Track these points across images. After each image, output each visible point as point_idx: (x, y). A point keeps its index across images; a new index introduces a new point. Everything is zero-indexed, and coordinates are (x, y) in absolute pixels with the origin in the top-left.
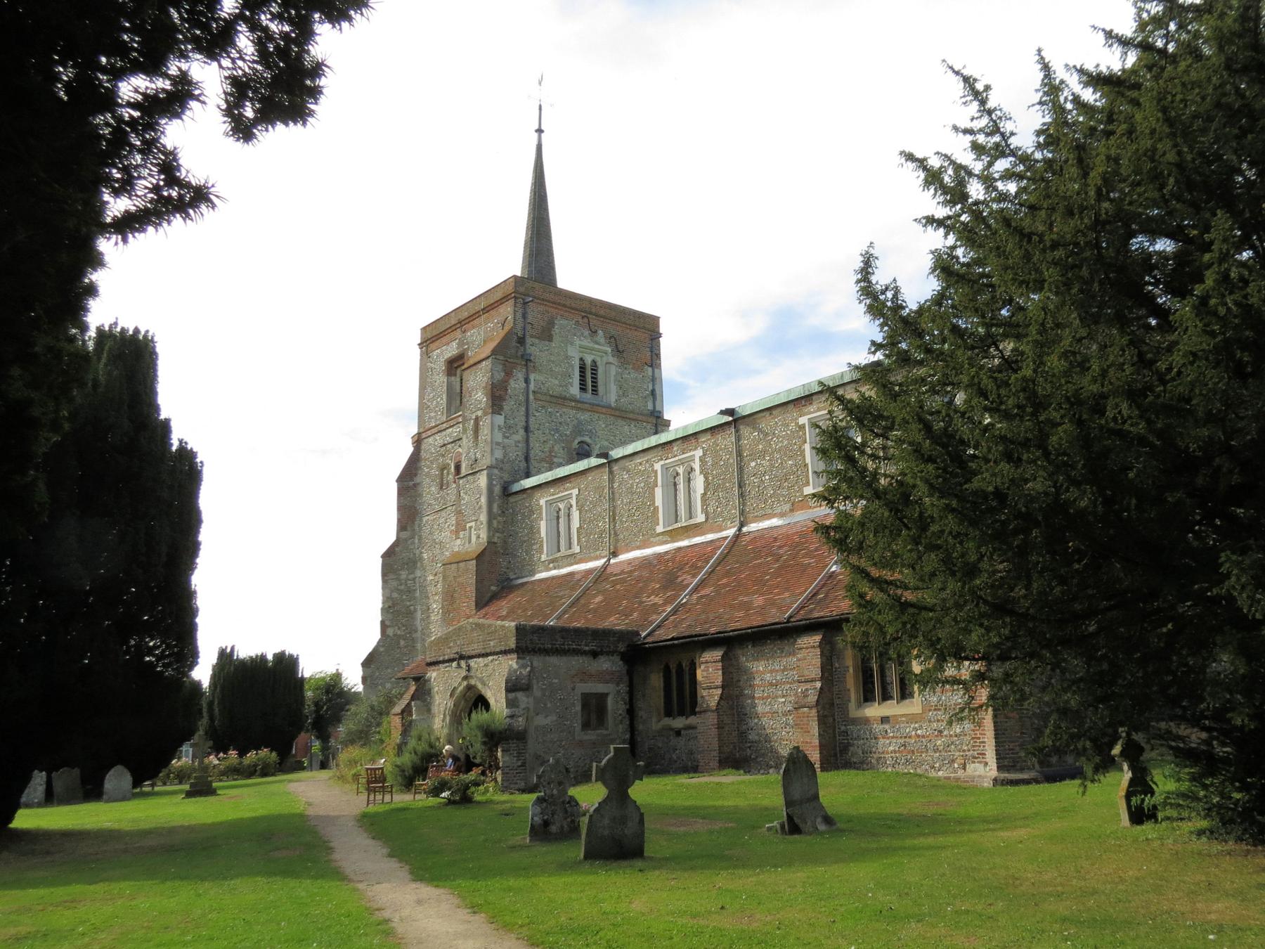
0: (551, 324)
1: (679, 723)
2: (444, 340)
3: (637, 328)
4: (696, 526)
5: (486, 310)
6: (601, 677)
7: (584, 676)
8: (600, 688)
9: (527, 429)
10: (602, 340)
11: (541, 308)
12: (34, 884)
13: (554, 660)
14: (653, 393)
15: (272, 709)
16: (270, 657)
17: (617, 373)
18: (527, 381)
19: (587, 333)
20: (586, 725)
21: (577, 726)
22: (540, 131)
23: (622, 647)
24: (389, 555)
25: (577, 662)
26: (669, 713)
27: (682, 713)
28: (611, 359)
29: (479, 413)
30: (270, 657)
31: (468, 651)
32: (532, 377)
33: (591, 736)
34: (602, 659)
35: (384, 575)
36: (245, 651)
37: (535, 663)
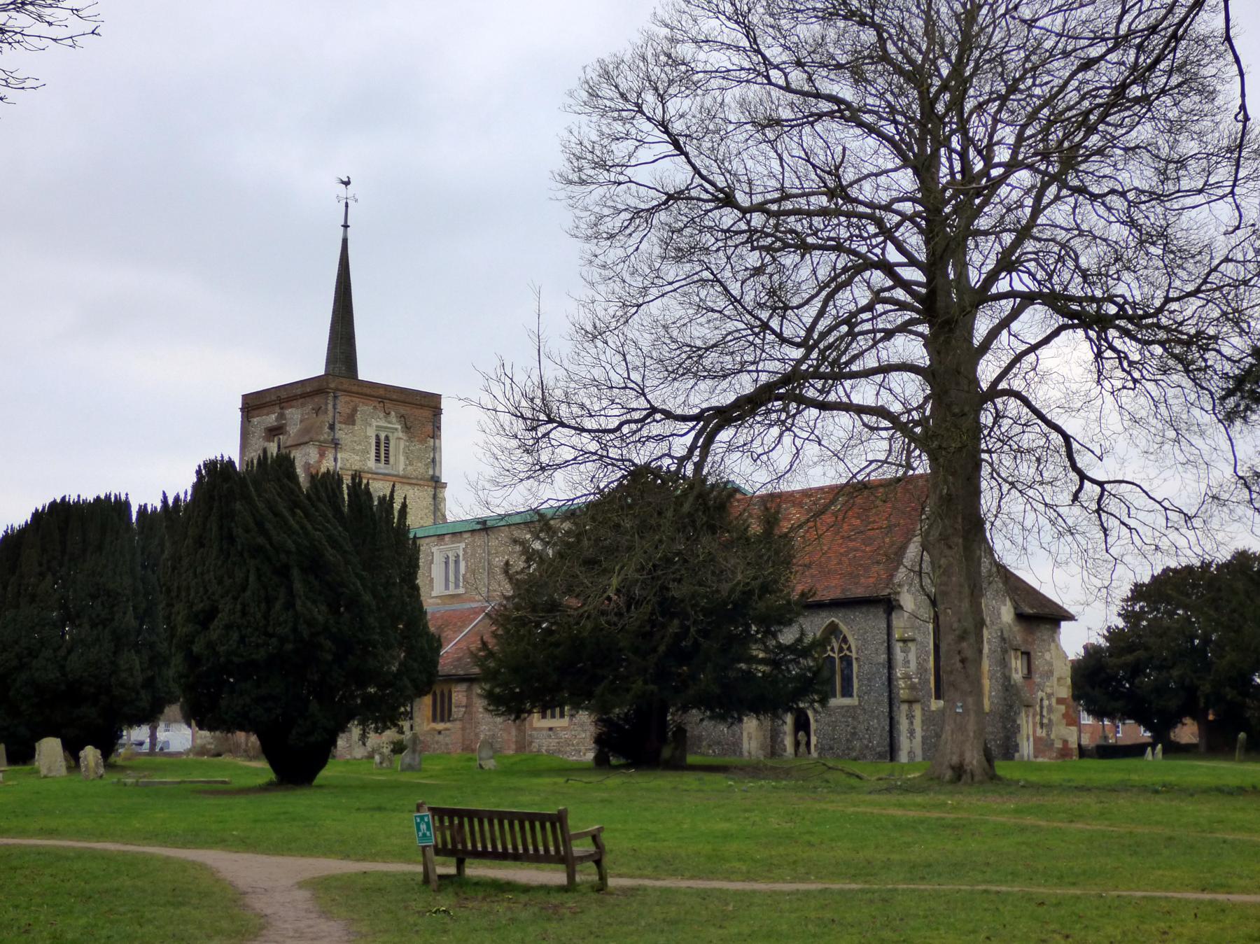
0: (355, 410)
1: (440, 726)
2: (265, 411)
3: (422, 406)
4: (459, 595)
5: (304, 396)
10: (394, 420)
11: (348, 399)
12: (506, 867)
14: (434, 461)
16: (1121, 623)
17: (406, 446)
18: (335, 460)
19: (382, 415)
26: (434, 720)
27: (442, 720)
28: (401, 435)
30: (1121, 623)
32: (339, 456)
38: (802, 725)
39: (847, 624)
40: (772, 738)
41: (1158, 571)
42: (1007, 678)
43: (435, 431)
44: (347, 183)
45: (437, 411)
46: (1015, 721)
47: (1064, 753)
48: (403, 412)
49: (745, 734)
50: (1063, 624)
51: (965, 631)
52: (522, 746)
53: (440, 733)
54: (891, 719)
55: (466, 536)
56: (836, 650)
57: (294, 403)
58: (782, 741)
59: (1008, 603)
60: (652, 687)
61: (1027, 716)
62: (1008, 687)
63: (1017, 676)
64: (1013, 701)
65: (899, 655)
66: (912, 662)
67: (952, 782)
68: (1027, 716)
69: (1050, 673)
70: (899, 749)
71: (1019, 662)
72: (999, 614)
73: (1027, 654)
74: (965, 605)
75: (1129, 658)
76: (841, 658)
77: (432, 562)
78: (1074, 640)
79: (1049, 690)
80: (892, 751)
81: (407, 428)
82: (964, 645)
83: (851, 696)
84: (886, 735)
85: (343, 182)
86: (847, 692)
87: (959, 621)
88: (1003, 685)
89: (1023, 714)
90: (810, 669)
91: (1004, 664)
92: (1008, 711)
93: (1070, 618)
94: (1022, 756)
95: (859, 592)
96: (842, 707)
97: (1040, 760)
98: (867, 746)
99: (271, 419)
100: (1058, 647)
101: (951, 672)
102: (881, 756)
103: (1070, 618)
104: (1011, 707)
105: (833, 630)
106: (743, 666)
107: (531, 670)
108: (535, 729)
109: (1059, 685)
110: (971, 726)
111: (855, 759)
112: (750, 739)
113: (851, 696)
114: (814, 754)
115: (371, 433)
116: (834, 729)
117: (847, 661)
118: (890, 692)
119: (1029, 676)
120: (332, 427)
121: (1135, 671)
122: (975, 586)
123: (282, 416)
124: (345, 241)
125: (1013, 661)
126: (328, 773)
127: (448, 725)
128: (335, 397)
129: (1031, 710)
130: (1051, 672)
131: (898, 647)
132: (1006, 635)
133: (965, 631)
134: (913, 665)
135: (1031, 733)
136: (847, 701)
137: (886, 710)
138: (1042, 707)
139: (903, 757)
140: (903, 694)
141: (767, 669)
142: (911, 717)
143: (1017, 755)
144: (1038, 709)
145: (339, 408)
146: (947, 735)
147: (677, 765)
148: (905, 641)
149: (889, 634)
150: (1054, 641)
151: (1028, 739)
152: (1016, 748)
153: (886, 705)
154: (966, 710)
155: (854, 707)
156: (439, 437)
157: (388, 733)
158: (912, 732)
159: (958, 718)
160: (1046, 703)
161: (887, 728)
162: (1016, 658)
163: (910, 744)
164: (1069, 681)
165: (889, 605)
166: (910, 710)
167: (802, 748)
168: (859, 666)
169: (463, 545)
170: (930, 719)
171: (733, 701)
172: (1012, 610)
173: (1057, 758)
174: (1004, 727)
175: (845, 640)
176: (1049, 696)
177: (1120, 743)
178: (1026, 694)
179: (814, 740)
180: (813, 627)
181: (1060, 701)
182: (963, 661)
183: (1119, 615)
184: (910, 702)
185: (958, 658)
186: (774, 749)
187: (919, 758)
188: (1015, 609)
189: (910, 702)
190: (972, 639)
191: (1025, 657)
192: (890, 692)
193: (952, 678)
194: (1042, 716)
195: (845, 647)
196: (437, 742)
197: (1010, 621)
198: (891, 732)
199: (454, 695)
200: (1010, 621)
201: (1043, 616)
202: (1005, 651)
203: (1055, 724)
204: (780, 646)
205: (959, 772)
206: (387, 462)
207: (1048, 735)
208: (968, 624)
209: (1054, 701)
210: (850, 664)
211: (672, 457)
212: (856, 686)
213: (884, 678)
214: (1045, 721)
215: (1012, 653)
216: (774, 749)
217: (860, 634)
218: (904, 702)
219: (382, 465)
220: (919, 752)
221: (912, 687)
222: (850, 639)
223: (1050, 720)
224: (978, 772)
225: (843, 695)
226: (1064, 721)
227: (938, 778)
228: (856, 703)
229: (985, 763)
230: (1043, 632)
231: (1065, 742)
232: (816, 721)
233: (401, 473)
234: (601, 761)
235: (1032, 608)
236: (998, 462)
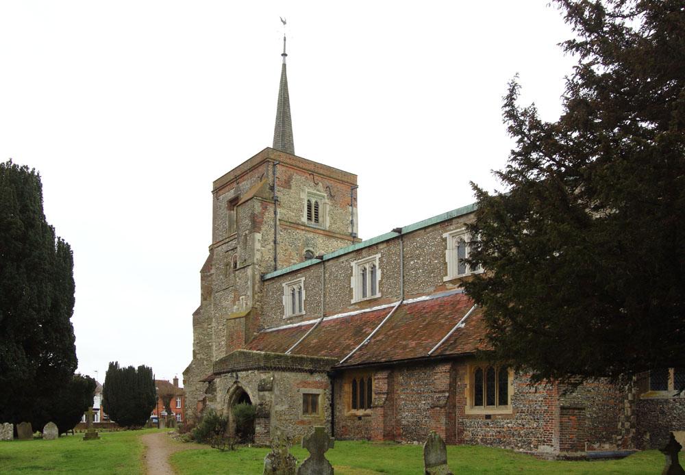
1: (360, 412)
2: (227, 189)
6: (316, 385)
7: (305, 384)
10: (322, 189)
13: (287, 374)
14: (352, 222)
15: (133, 394)
16: (136, 368)
19: (312, 184)
21: (300, 412)
22: (284, 55)
23: (328, 369)
24: (196, 314)
25: (300, 376)
26: (355, 407)
27: (362, 407)
28: (327, 201)
29: (247, 232)
30: (136, 368)
31: (237, 367)
32: (278, 210)
33: (307, 418)
35: (194, 326)
36: (123, 364)
37: (276, 376)
43: (353, 201)
45: (354, 187)
48: (328, 184)
53: (360, 418)
55: (381, 247)
57: (246, 177)
77: (351, 275)
81: (331, 196)
99: (230, 194)
108: (468, 417)
115: (304, 196)
120: (272, 188)
123: (237, 189)
124: (284, 66)
127: (368, 411)
128: (274, 165)
145: (278, 175)
147: (269, 413)
156: (356, 206)
157: (212, 407)
169: (379, 255)
199: (374, 383)
206: (317, 220)
219: (313, 222)
233: (327, 229)
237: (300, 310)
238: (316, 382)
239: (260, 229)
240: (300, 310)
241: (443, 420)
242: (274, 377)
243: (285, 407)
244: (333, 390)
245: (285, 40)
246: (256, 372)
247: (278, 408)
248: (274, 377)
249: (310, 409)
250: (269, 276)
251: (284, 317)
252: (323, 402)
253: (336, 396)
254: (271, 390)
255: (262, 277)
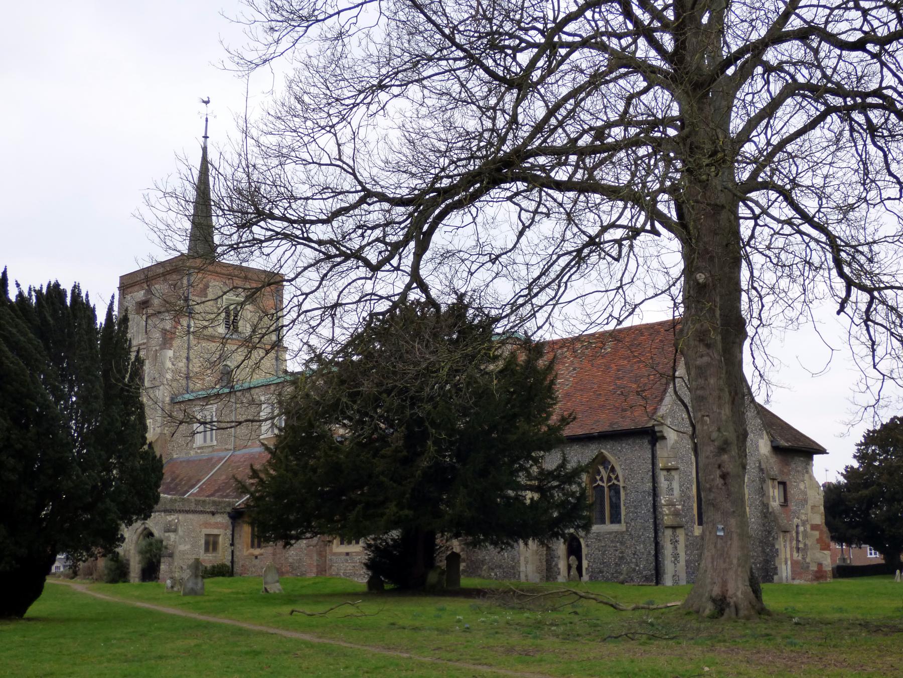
6: (216, 526)
7: (206, 525)
8: (215, 532)
9: (188, 359)
13: (190, 516)
16: (856, 465)
20: (207, 550)
21: (202, 551)
22: (206, 137)
23: (229, 509)
25: (202, 518)
26: (252, 546)
29: (158, 348)
30: (856, 465)
34: (217, 516)
37: (180, 518)
38: (574, 549)
39: (614, 455)
40: (547, 561)
41: (886, 420)
42: (766, 506)
44: (207, 102)
46: (773, 546)
47: (819, 575)
49: (522, 558)
50: (816, 457)
51: (726, 442)
52: (322, 570)
53: (256, 557)
54: (657, 544)
56: (605, 479)
58: (557, 565)
59: (765, 436)
60: (406, 512)
61: (785, 541)
62: (766, 513)
63: (775, 504)
64: (772, 527)
65: (663, 483)
66: (676, 490)
67: (712, 617)
68: (785, 541)
69: (805, 501)
70: (664, 573)
71: (776, 491)
72: (757, 447)
73: (783, 484)
74: (726, 411)
75: (865, 492)
76: (609, 487)
78: (829, 470)
79: (803, 517)
80: (657, 576)
82: (725, 457)
83: (619, 522)
84: (652, 558)
85: (204, 102)
86: (615, 518)
87: (719, 430)
88: (762, 512)
89: (781, 539)
90: (573, 494)
91: (762, 492)
92: (767, 537)
93: (822, 451)
94: (781, 578)
95: (626, 424)
96: (610, 533)
97: (797, 582)
98: (634, 570)
99: (140, 295)
100: (811, 478)
101: (710, 490)
102: (647, 579)
103: (822, 451)
104: (769, 532)
105: (601, 460)
106: (511, 493)
107: (293, 497)
108: (335, 554)
109: (813, 513)
110: (735, 552)
111: (622, 583)
112: (527, 563)
113: (619, 522)
114: (585, 577)
116: (603, 554)
117: (615, 489)
118: (655, 518)
119: (785, 503)
121: (871, 502)
122: (736, 394)
123: (149, 291)
125: (771, 490)
126: (33, 610)
129: (788, 535)
130: (806, 501)
131: (662, 476)
132: (763, 466)
133: (726, 442)
134: (677, 492)
135: (789, 556)
136: (615, 527)
137: (652, 535)
138: (797, 533)
139: (668, 581)
140: (667, 520)
141: (536, 496)
142: (675, 542)
143: (776, 577)
144: (794, 535)
146: (706, 563)
147: (449, 588)
148: (668, 470)
149: (654, 464)
150: (807, 472)
151: (786, 563)
152: (775, 570)
153: (652, 531)
154: (728, 534)
155: (622, 533)
158: (676, 557)
159: (719, 541)
160: (801, 529)
161: (653, 552)
162: (774, 487)
163: (674, 567)
164: (822, 508)
165: (652, 436)
166: (674, 535)
167: (574, 572)
168: (626, 494)
170: (696, 546)
171: (506, 525)
172: (769, 443)
173: (812, 580)
174: (763, 551)
175: (613, 470)
176: (804, 523)
177: (854, 564)
178: (783, 521)
179: (585, 564)
180: (578, 456)
181: (814, 527)
182: (724, 476)
183: (855, 457)
184: (674, 528)
185: (718, 473)
186: (549, 572)
187: (683, 582)
188: (772, 442)
189: (674, 528)
190: (734, 451)
191: (781, 487)
192: (655, 518)
193: (712, 496)
194: (798, 541)
195: (613, 477)
196: (254, 566)
197: (767, 453)
198: (656, 556)
200: (767, 453)
201: (799, 450)
202: (763, 481)
203: (805, 550)
204: (542, 471)
205: (721, 605)
207: (804, 558)
208: (730, 434)
209: (808, 527)
210: (617, 492)
211: (386, 244)
212: (623, 513)
213: (650, 505)
214: (801, 546)
215: (770, 482)
216: (549, 572)
217: (627, 463)
218: (667, 527)
220: (683, 575)
221: (676, 514)
222: (617, 468)
223: (805, 545)
224: (743, 605)
225: (612, 522)
226: (818, 546)
227: (697, 612)
228: (624, 529)
229: (752, 595)
230: (797, 463)
231: (820, 565)
232: (587, 546)
234: (375, 588)
235: (787, 441)
236: (757, 269)
237: (212, 440)
238: (217, 523)
239: (172, 346)
240: (212, 440)
241: (315, 557)
242: (178, 519)
243: (188, 547)
244: (233, 531)
245: (207, 121)
246: (163, 514)
247: (182, 548)
248: (178, 519)
249: (211, 548)
250: (180, 399)
251: (195, 446)
252: (223, 541)
253: (236, 536)
254: (175, 531)
255: (172, 399)
